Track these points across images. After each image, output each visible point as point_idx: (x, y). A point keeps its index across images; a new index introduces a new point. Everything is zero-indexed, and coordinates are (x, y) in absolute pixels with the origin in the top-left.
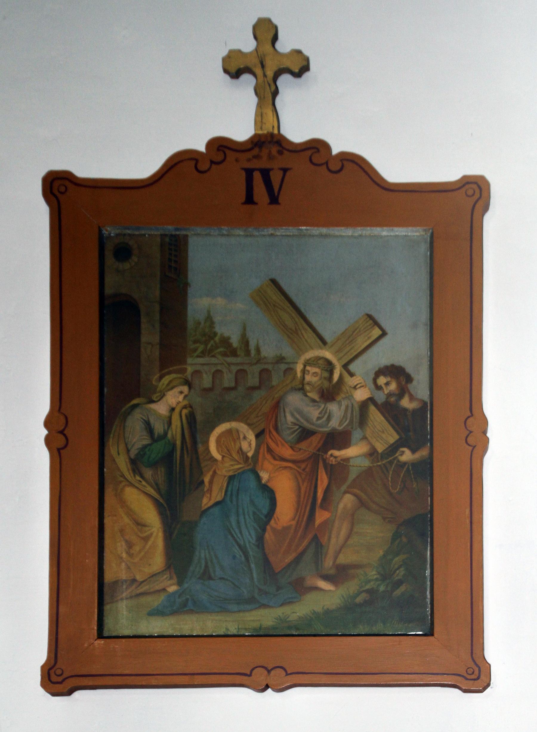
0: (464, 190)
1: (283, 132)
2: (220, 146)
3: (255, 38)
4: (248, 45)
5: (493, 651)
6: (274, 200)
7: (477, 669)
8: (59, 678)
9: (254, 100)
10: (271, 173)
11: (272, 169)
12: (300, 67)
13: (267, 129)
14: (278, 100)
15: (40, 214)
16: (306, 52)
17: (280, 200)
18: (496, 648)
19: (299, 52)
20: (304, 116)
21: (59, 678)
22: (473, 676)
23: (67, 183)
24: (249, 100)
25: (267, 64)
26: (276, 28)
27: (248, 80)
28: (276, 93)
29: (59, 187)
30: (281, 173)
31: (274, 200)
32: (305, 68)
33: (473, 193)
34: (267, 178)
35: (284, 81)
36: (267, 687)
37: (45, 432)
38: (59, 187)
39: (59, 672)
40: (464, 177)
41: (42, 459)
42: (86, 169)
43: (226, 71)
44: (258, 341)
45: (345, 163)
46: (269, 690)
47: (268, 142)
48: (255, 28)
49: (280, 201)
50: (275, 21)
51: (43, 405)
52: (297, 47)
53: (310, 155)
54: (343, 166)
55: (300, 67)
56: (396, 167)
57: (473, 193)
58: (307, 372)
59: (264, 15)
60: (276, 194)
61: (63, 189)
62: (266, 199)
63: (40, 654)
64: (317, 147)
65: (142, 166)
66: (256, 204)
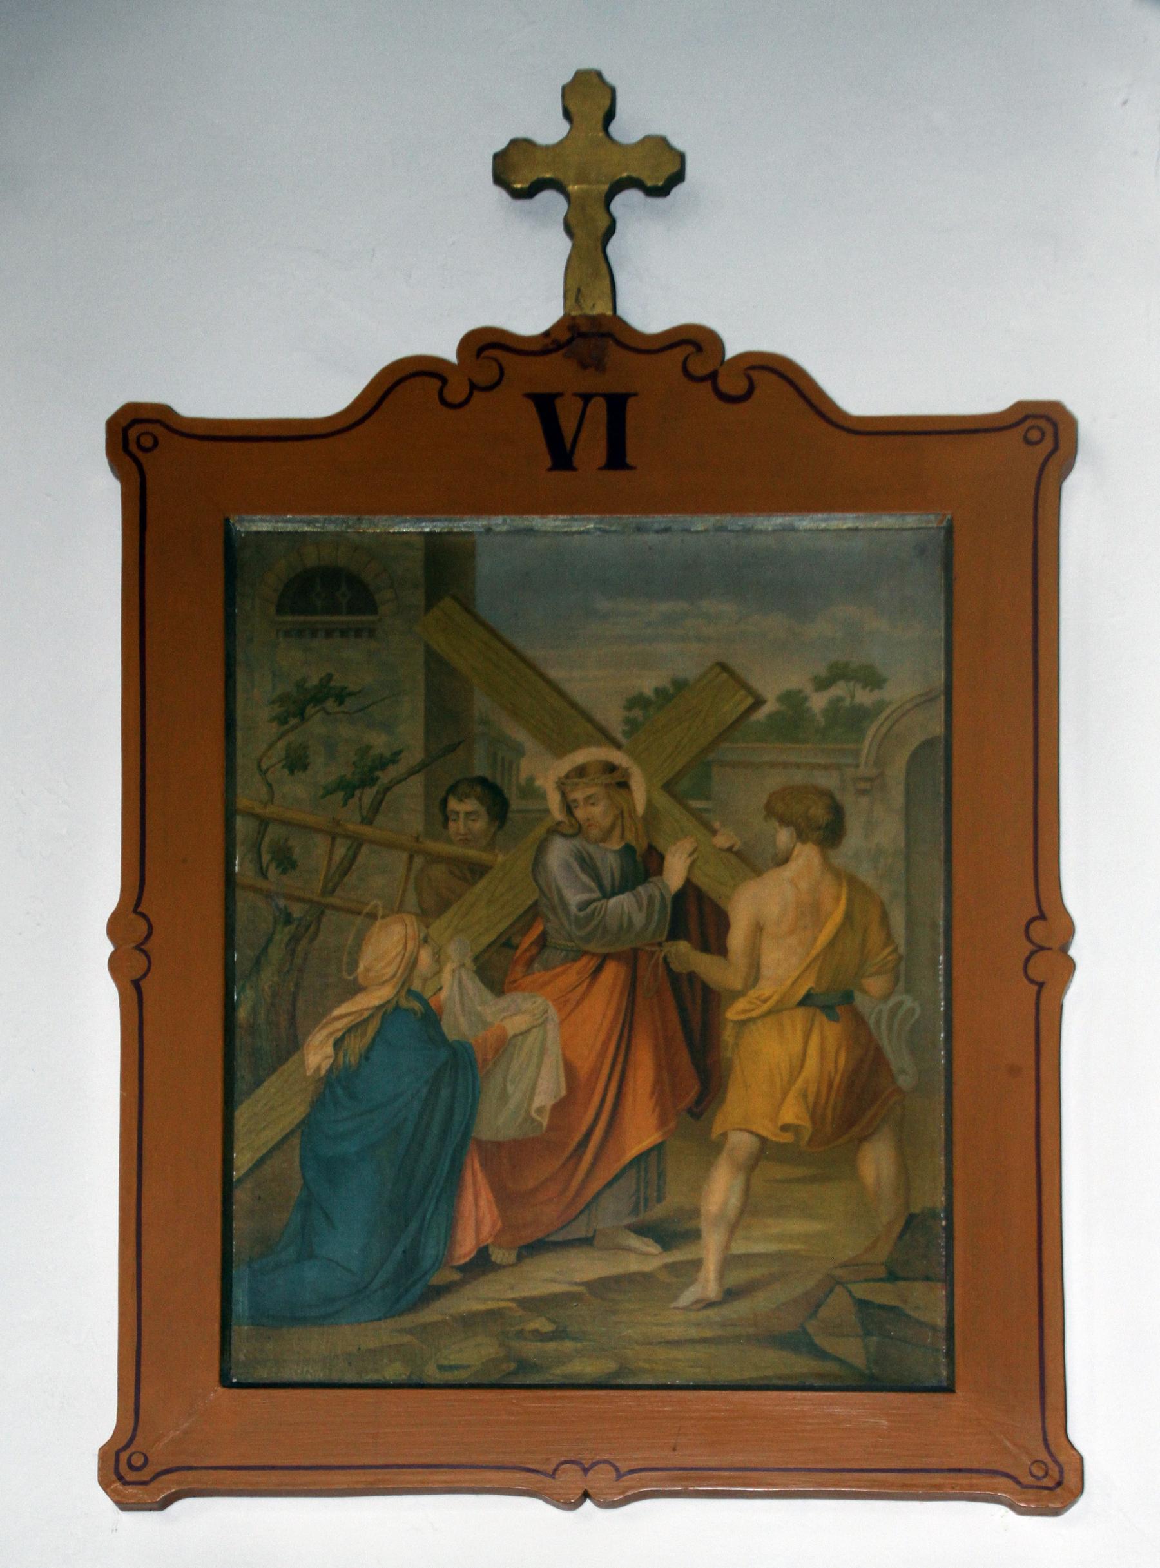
0: (1021, 430)
1: (620, 312)
2: (486, 345)
3: (567, 114)
4: (550, 129)
5: (1085, 1426)
6: (617, 459)
7: (1057, 1469)
8: (138, 1472)
9: (564, 245)
10: (559, 403)
11: (560, 395)
12: (661, 173)
13: (601, 308)
14: (614, 248)
15: (103, 496)
16: (677, 143)
17: (577, 460)
18: (1093, 1417)
19: (662, 142)
20: (664, 282)
21: (138, 1472)
22: (1049, 1481)
23: (157, 429)
24: (557, 247)
25: (590, 169)
26: (613, 91)
27: (552, 203)
28: (611, 230)
29: (142, 440)
30: (579, 404)
31: (617, 459)
32: (678, 177)
33: (1041, 437)
34: (596, 408)
35: (627, 203)
36: (586, 1495)
37: (109, 948)
38: (142, 440)
39: (138, 1461)
40: (1020, 405)
41: (103, 1004)
42: (198, 401)
43: (500, 178)
44: (459, 744)
45: (755, 374)
46: (588, 1504)
47: (591, 332)
48: (565, 91)
49: (576, 463)
50: (610, 77)
51: (107, 890)
52: (656, 130)
53: (682, 359)
54: (751, 389)
55: (661, 173)
56: (866, 382)
57: (1041, 437)
58: (573, 805)
59: (589, 63)
60: (568, 446)
61: (147, 442)
62: (600, 453)
63: (102, 1420)
64: (694, 342)
65: (322, 391)
66: (529, 396)
